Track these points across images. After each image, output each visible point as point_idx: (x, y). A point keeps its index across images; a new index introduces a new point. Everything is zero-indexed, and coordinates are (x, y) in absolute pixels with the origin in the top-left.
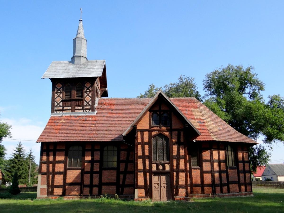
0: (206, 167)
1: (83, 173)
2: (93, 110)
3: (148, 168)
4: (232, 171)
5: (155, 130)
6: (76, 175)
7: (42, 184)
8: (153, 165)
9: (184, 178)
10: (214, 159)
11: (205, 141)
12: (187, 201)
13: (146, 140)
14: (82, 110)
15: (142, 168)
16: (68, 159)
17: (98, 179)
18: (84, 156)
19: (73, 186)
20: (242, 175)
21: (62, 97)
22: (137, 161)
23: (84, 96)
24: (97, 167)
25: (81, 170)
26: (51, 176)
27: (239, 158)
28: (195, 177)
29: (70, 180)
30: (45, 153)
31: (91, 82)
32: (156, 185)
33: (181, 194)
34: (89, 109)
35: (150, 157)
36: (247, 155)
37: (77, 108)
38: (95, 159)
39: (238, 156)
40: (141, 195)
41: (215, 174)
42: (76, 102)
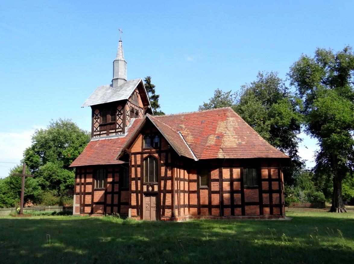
0: (215, 186)
1: (106, 194)
3: (139, 189)
4: (250, 190)
5: (146, 153)
6: (101, 196)
9: (171, 199)
10: (223, 178)
12: (172, 222)
13: (139, 163)
14: (115, 133)
16: (200, 177)
17: (117, 199)
18: (107, 178)
19: (98, 205)
22: (131, 183)
23: (117, 119)
24: (117, 187)
25: (104, 191)
26: (82, 196)
27: (262, 176)
28: (202, 198)
29: (96, 200)
30: (78, 176)
31: (122, 105)
32: (148, 205)
33: (167, 215)
34: (121, 132)
36: (276, 172)
37: (111, 131)
38: (115, 181)
39: (261, 173)
40: (134, 214)
41: (224, 194)
42: (110, 126)
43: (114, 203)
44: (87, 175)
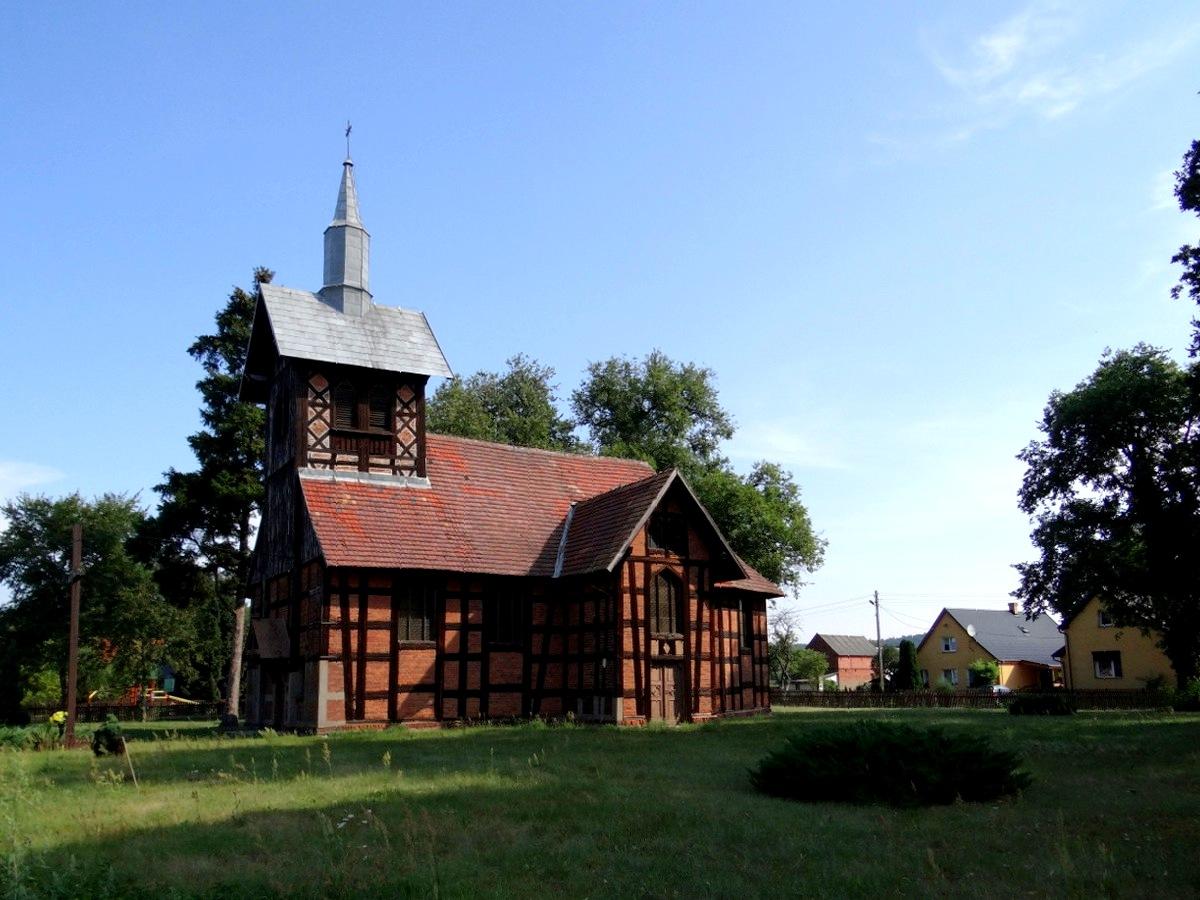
1: (442, 657)
2: (422, 474)
3: (642, 649)
7: (332, 688)
8: (653, 642)
9: (709, 674)
11: (381, 569)
13: (640, 583)
15: (631, 650)
20: (757, 667)
21: (329, 421)
23: (396, 427)
24: (475, 646)
31: (413, 387)
35: (646, 624)
43: (469, 688)
44: (370, 597)
